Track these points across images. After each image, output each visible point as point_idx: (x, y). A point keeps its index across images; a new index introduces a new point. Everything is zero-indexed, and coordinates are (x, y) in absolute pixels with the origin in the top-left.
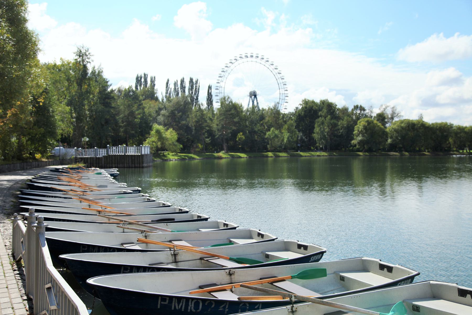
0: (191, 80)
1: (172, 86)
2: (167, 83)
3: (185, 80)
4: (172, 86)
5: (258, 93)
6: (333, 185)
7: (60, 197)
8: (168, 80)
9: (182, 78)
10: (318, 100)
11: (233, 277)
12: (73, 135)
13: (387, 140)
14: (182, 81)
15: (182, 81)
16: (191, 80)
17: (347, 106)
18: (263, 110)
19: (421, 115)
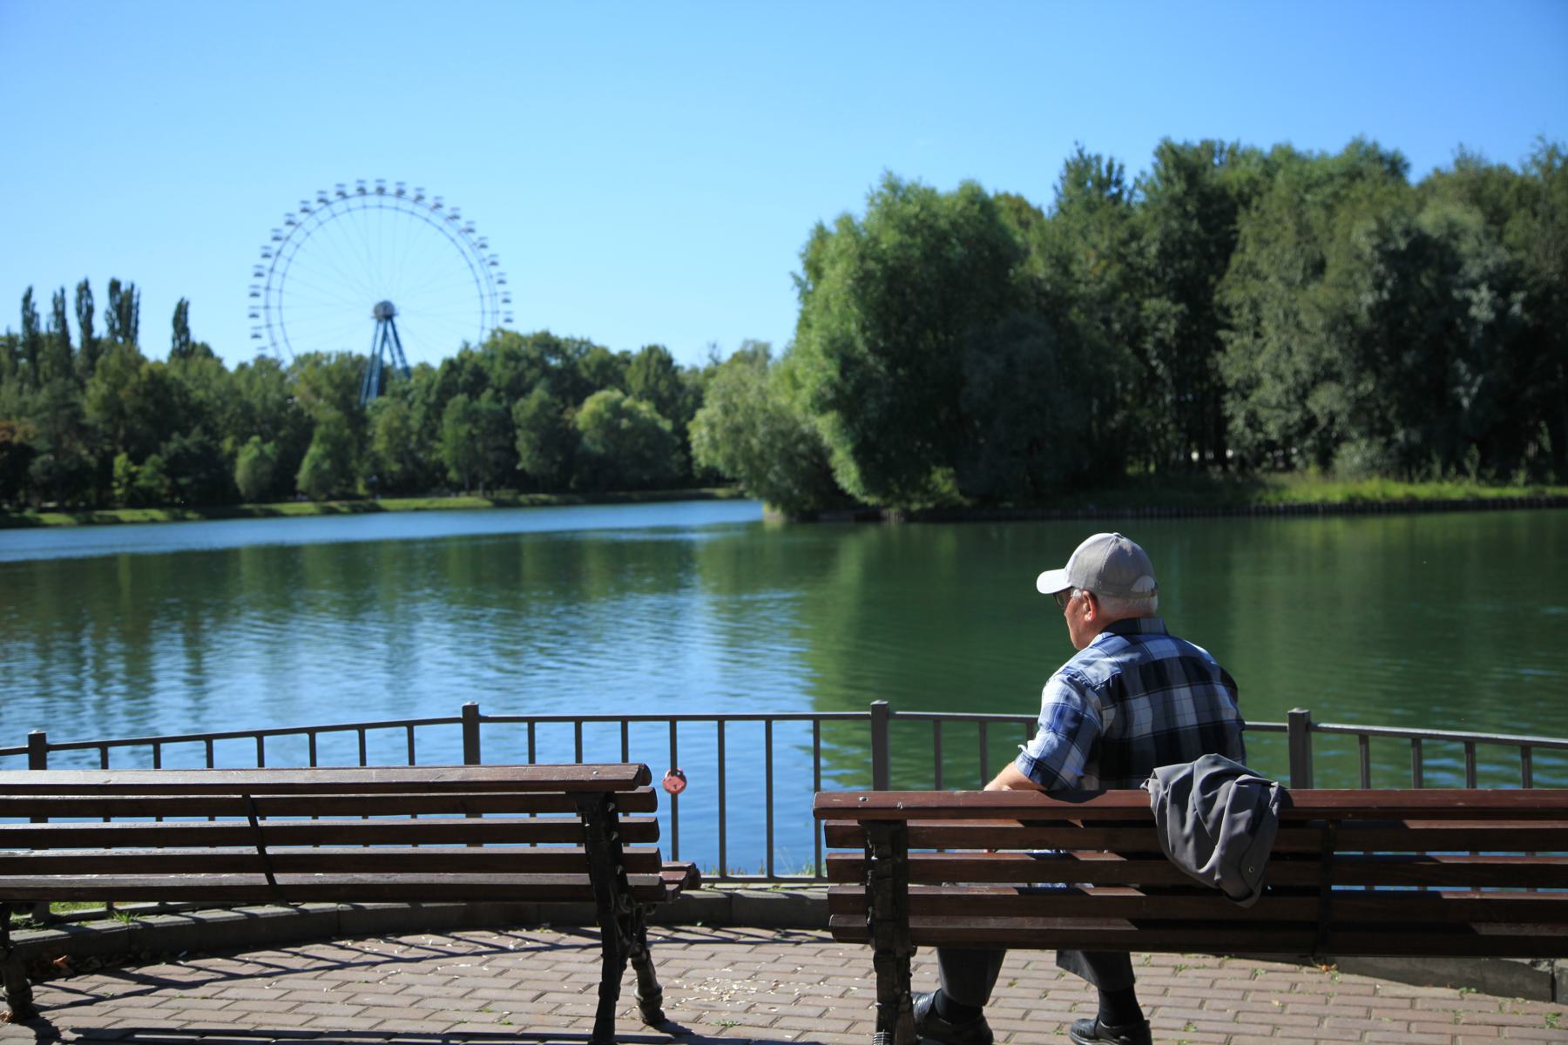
0: (115, 286)
1: (44, 309)
2: (27, 299)
3: (92, 287)
4: (44, 309)
5: (398, 304)
6: (478, 602)
7: (113, 997)
8: (30, 291)
9: (81, 279)
10: (615, 350)
11: (688, 840)
12: (83, 626)
13: (1459, 405)
14: (84, 290)
15: (84, 290)
16: (115, 286)
17: (763, 338)
18: (484, 346)
19: (1461, 145)
